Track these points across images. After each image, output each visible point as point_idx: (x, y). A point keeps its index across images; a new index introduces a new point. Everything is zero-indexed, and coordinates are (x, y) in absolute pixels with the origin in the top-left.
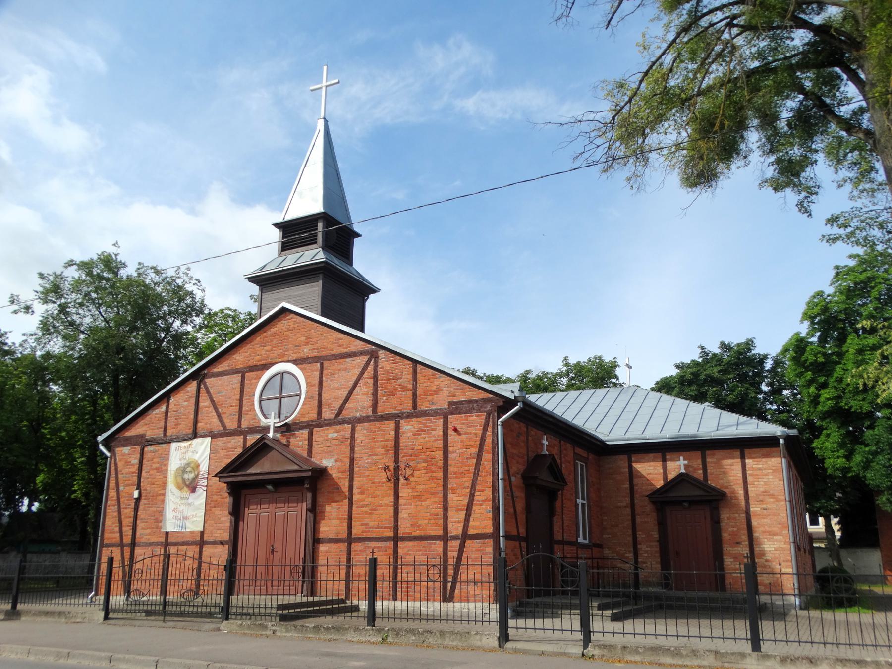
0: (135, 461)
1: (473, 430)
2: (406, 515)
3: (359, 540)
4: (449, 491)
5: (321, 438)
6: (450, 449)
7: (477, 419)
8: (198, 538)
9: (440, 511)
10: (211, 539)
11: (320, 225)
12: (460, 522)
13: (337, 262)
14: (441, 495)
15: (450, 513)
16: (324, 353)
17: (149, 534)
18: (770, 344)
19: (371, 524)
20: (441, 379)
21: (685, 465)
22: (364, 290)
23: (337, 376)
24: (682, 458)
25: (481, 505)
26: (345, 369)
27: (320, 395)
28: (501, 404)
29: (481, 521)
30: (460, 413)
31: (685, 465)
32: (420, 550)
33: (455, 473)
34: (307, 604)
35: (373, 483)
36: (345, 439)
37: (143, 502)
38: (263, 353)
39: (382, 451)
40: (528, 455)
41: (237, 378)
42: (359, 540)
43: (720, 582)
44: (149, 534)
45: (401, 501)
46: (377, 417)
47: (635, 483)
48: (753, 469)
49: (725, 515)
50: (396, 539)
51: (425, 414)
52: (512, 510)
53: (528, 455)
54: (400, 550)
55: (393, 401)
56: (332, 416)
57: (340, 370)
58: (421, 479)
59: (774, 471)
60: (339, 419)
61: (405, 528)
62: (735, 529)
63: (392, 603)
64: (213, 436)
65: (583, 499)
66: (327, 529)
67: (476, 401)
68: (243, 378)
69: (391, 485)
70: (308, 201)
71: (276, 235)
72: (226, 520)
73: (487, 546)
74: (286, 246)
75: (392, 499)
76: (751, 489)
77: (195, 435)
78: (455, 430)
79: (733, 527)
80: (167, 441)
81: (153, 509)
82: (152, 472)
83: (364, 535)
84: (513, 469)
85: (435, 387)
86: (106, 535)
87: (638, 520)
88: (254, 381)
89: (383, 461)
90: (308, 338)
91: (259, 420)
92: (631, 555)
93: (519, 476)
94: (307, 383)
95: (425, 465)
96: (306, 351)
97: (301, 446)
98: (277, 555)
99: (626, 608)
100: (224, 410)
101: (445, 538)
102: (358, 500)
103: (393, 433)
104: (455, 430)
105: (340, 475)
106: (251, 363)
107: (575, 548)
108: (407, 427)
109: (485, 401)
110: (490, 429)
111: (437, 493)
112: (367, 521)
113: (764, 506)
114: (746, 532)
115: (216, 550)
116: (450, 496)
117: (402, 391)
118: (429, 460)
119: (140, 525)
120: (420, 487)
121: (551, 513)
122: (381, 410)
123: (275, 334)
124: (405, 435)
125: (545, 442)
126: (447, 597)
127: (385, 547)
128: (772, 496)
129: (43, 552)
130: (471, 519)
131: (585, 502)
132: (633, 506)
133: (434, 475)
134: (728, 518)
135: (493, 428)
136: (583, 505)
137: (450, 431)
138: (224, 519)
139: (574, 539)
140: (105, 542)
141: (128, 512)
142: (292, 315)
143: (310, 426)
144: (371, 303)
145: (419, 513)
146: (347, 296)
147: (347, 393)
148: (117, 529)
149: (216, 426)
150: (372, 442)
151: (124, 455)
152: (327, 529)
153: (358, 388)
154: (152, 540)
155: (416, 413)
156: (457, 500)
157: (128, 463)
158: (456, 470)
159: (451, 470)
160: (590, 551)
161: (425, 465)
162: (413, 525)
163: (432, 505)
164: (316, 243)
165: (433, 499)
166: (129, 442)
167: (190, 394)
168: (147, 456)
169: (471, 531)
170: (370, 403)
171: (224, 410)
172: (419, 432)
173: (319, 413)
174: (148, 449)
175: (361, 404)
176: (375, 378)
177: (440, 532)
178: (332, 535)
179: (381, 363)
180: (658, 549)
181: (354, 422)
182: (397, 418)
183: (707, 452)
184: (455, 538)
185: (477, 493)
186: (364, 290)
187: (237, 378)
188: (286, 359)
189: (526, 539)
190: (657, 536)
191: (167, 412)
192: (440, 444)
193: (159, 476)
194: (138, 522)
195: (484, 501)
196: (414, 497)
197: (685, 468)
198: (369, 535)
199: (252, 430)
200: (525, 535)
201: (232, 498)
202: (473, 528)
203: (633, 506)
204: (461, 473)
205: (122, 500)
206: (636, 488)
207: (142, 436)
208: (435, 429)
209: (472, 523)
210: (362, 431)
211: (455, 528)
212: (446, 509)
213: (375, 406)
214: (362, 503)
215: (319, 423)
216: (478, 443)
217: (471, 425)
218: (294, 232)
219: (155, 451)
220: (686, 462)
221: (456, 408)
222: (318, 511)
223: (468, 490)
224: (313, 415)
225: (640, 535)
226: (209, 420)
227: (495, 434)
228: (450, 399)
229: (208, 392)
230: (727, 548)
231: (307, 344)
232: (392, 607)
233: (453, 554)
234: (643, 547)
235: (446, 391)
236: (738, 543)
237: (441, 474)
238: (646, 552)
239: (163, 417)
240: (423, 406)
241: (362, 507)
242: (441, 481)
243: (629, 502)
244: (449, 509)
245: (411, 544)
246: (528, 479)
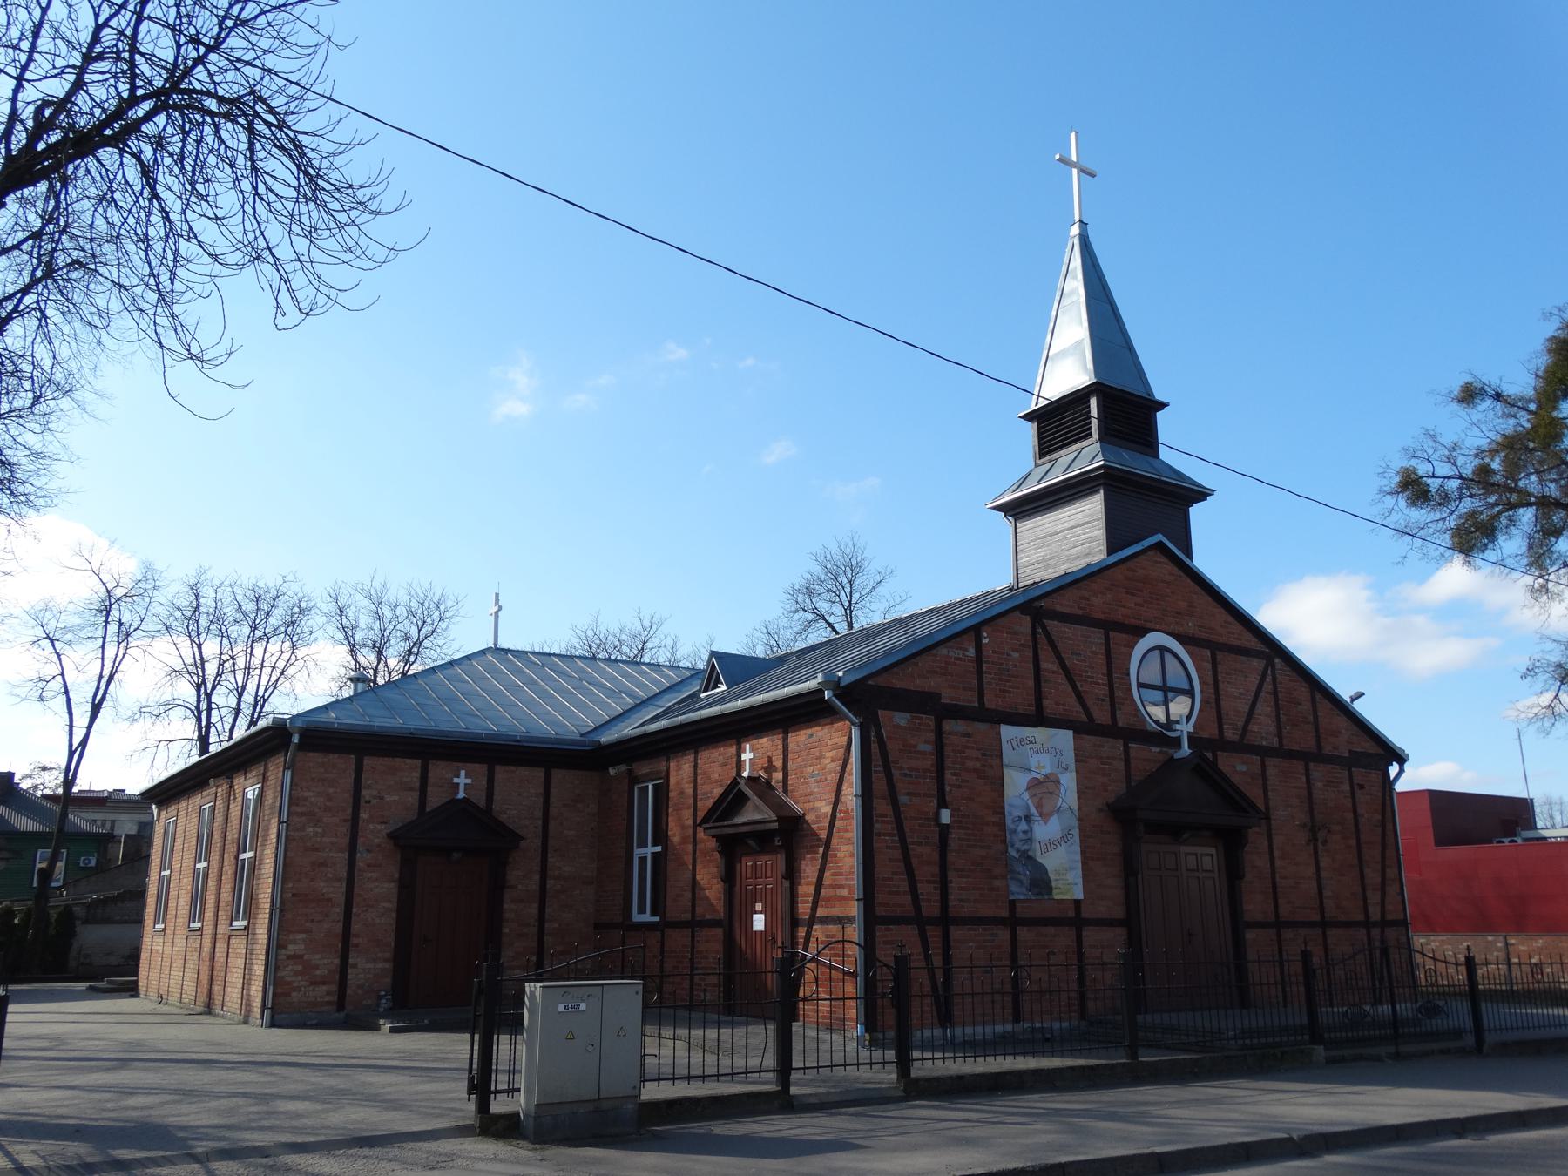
11: (1093, 402)
13: (1131, 462)
15: (1369, 894)
18: (1419, 774)
24: (463, 773)
70: (1067, 370)
71: (1029, 433)
74: (1047, 447)
126: (1017, 1018)
129: (888, 654)
148: (905, 887)
218: (1056, 423)
220: (469, 781)
226: (1058, 697)
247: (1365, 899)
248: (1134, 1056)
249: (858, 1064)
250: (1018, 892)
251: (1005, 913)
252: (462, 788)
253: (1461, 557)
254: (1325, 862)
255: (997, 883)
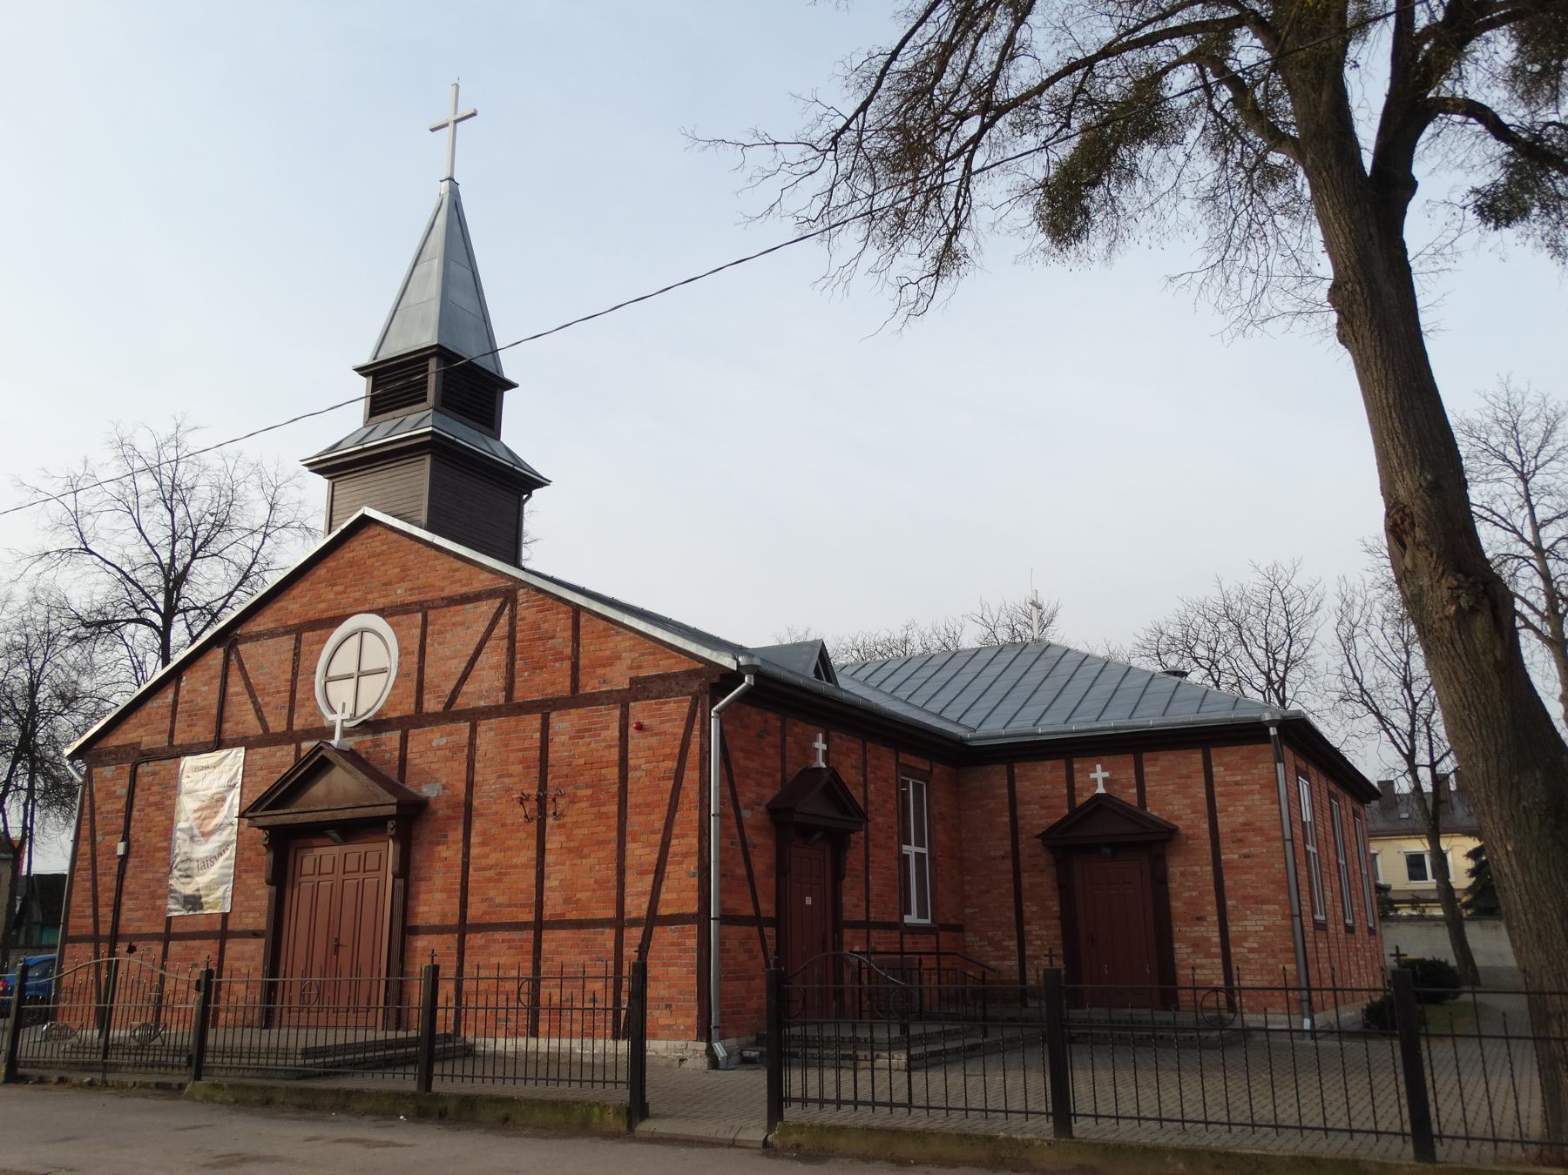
0: (122, 791)
1: (668, 727)
2: (556, 883)
3: (480, 928)
4: (628, 838)
5: (422, 748)
6: (631, 762)
7: (676, 709)
8: (219, 927)
9: (612, 874)
10: (240, 928)
12: (644, 893)
13: (465, 435)
14: (614, 846)
15: (630, 878)
16: (428, 596)
17: (140, 920)
19: (499, 900)
20: (619, 638)
21: (1104, 779)
22: (523, 482)
23: (448, 636)
24: (1099, 767)
25: (680, 863)
26: (462, 624)
27: (421, 670)
28: (716, 680)
29: (679, 894)
30: (648, 698)
31: (1104, 779)
32: (577, 946)
33: (637, 806)
34: (387, 1045)
35: (503, 825)
36: (461, 749)
37: (132, 862)
38: (331, 596)
39: (518, 769)
40: (783, 769)
41: (288, 643)
42: (480, 928)
43: (1167, 995)
44: (140, 920)
45: (549, 858)
46: (511, 708)
47: (1019, 813)
48: (1226, 784)
49: (1175, 868)
50: (539, 926)
51: (593, 700)
52: (741, 871)
53: (783, 769)
54: (544, 946)
55: (540, 679)
56: (440, 708)
57: (454, 625)
58: (581, 819)
59: (1262, 786)
60: (450, 714)
61: (554, 904)
62: (1194, 894)
63: (532, 1041)
64: (249, 743)
65: (920, 843)
66: (426, 909)
67: (675, 675)
68: (298, 641)
69: (533, 826)
72: (262, 894)
73: (689, 936)
74: (378, 406)
75: (533, 853)
76: (1222, 819)
77: (218, 744)
78: (640, 727)
79: (1190, 889)
80: (176, 752)
81: (150, 876)
82: (148, 810)
83: (487, 919)
84: (748, 794)
85: (608, 653)
86: (72, 922)
87: (1026, 880)
88: (315, 647)
89: (519, 787)
90: (404, 569)
91: (322, 716)
92: (1013, 944)
93: (761, 808)
94: (400, 650)
95: (589, 792)
96: (400, 594)
97: (388, 762)
98: (345, 955)
99: (969, 1042)
100: (267, 699)
101: (619, 923)
102: (480, 857)
103: (537, 735)
104: (640, 727)
105: (450, 813)
106: (313, 615)
107: (896, 934)
108: (562, 724)
109: (691, 674)
110: (697, 726)
111: (609, 842)
112: (492, 893)
113: (1246, 851)
114: (1213, 898)
115: (246, 948)
116: (630, 846)
117: (556, 660)
118: (596, 785)
119: (127, 903)
120: (581, 832)
121: (838, 874)
122: (519, 695)
123: (351, 564)
124: (557, 739)
125: (820, 745)
127: (521, 940)
128: (1260, 831)
130: (663, 889)
131: (924, 850)
132: (1015, 853)
133: (603, 809)
134: (1183, 874)
135: (703, 724)
136: (920, 857)
137: (632, 731)
138: (258, 892)
139: (896, 919)
140: (71, 933)
141: (108, 881)
142: (379, 529)
143: (405, 724)
144: (536, 509)
145: (576, 879)
146: (487, 496)
147: (464, 665)
148: (89, 911)
149: (252, 726)
150: (502, 753)
151: (104, 779)
152: (426, 909)
153: (482, 658)
154: (145, 930)
155: (575, 699)
156: (641, 853)
157: (110, 795)
158: (640, 800)
159: (631, 800)
160: (933, 938)
161: (589, 792)
162: (567, 901)
163: (599, 864)
164: (425, 400)
165: (602, 854)
166: (118, 756)
167: (212, 672)
168: (144, 781)
169: (663, 911)
170: (500, 683)
171: (267, 699)
172: (580, 733)
173: (419, 703)
174: (143, 769)
175: (486, 686)
176: (511, 637)
177: (611, 913)
178: (435, 921)
179: (522, 611)
180: (1059, 932)
181: (475, 716)
182: (545, 707)
183: (1145, 755)
184: (635, 922)
185: (673, 842)
186: (523, 482)
187: (288, 643)
188: (367, 607)
189: (775, 922)
190: (1056, 908)
191: (175, 703)
192: (614, 754)
193: (159, 817)
194: (124, 898)
195: (686, 855)
196: (570, 851)
197: (1105, 786)
198: (494, 919)
199: (308, 734)
200: (772, 914)
201: (271, 856)
202: (667, 904)
203: (1015, 853)
204: (648, 805)
205: (99, 859)
206: (1021, 822)
207: (135, 746)
208: (607, 728)
209: (665, 896)
210: (488, 734)
211: (636, 905)
212: (621, 872)
213: (510, 688)
214: (484, 862)
215: (419, 719)
216: (677, 751)
217: (665, 718)
219: (154, 773)
220: (1106, 774)
221: (641, 688)
222: (412, 877)
223: (659, 837)
224: (408, 707)
225: (1029, 908)
226: (243, 717)
227: (705, 733)
228: (633, 674)
229: (242, 667)
230: (1179, 928)
231: (403, 580)
232: (511, 1049)
233: (630, 953)
234: (1033, 929)
235: (627, 657)
236: (1199, 919)
237: (614, 808)
238: (1040, 937)
239: (167, 711)
240: (589, 686)
241: (484, 869)
242: (614, 822)
243: (1009, 848)
244: (628, 872)
245: (563, 934)
246: (782, 817)
247: (867, 880)
248: (426, 1080)
249: (928, 1108)
250: (175, 910)
251: (161, 929)
252: (1100, 783)
253: (1109, 181)
254: (552, 843)
255: (159, 902)
